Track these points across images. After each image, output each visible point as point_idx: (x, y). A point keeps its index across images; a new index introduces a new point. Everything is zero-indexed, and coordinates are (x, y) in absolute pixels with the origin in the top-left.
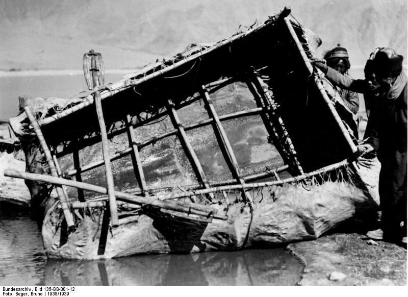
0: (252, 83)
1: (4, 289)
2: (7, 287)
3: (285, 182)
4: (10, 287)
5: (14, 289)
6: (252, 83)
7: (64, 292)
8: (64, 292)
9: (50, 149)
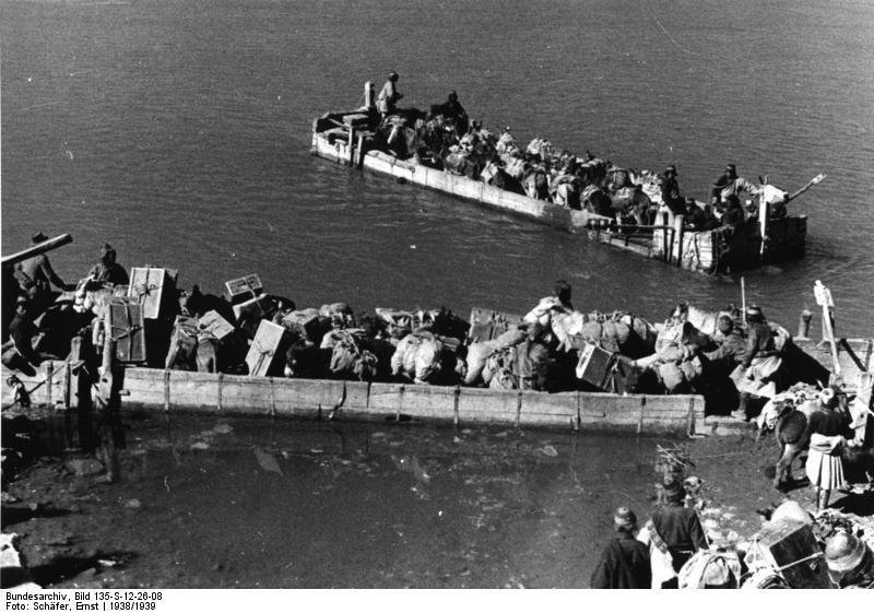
1: (8, 596)
5: (30, 597)
7: (145, 602)
8: (145, 602)
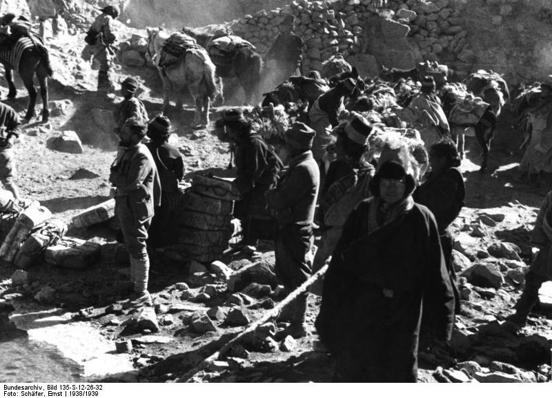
0: (224, 252)
1: (5, 387)
2: (9, 385)
3: (526, 90)
4: (14, 385)
5: (19, 388)
6: (224, 252)
7: (91, 391)
8: (91, 391)
9: (147, 334)
